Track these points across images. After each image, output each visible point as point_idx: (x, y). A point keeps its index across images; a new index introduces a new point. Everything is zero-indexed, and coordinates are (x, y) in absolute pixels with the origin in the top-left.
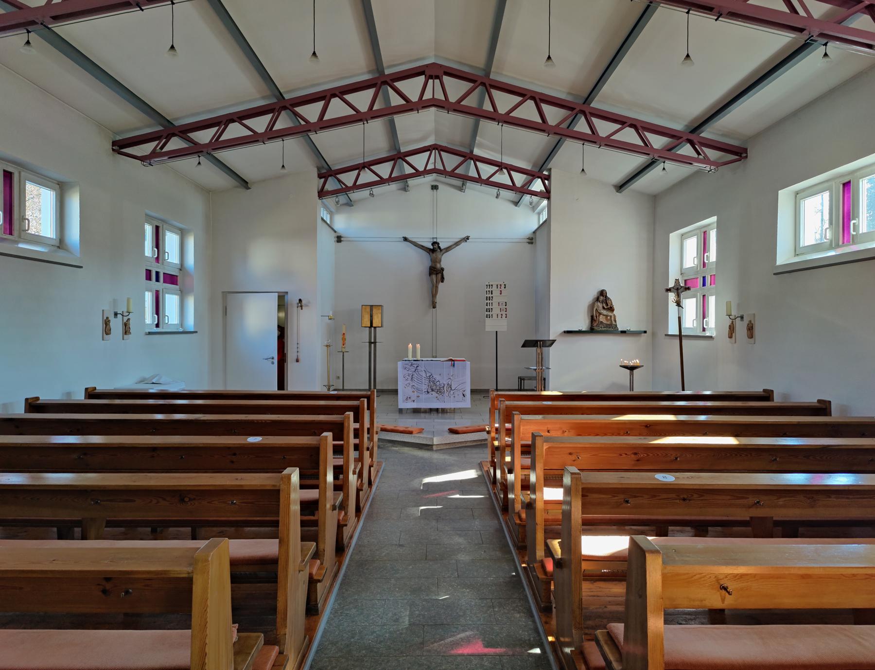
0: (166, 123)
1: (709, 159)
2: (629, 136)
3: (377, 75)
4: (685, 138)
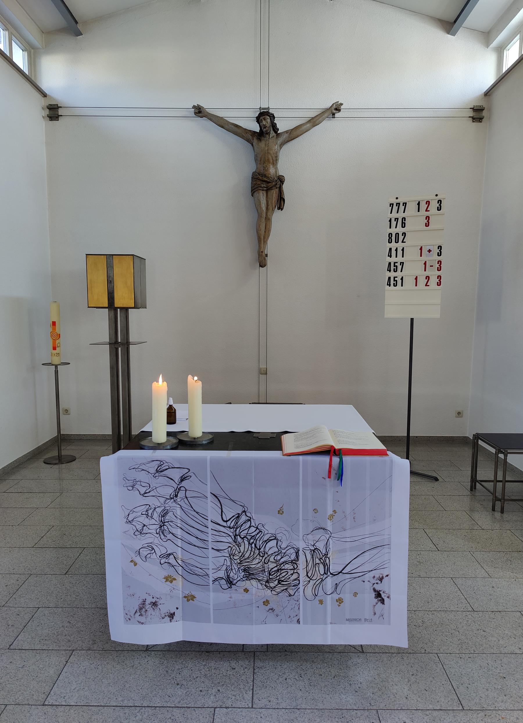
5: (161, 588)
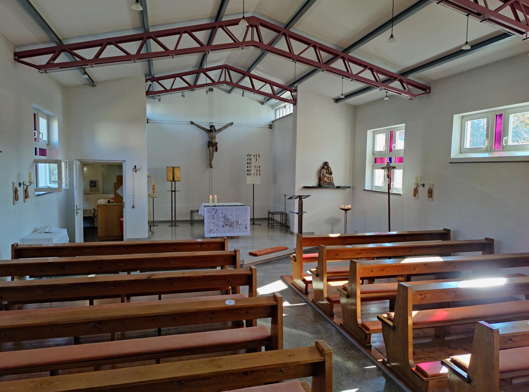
0: (58, 41)
5: (213, 228)
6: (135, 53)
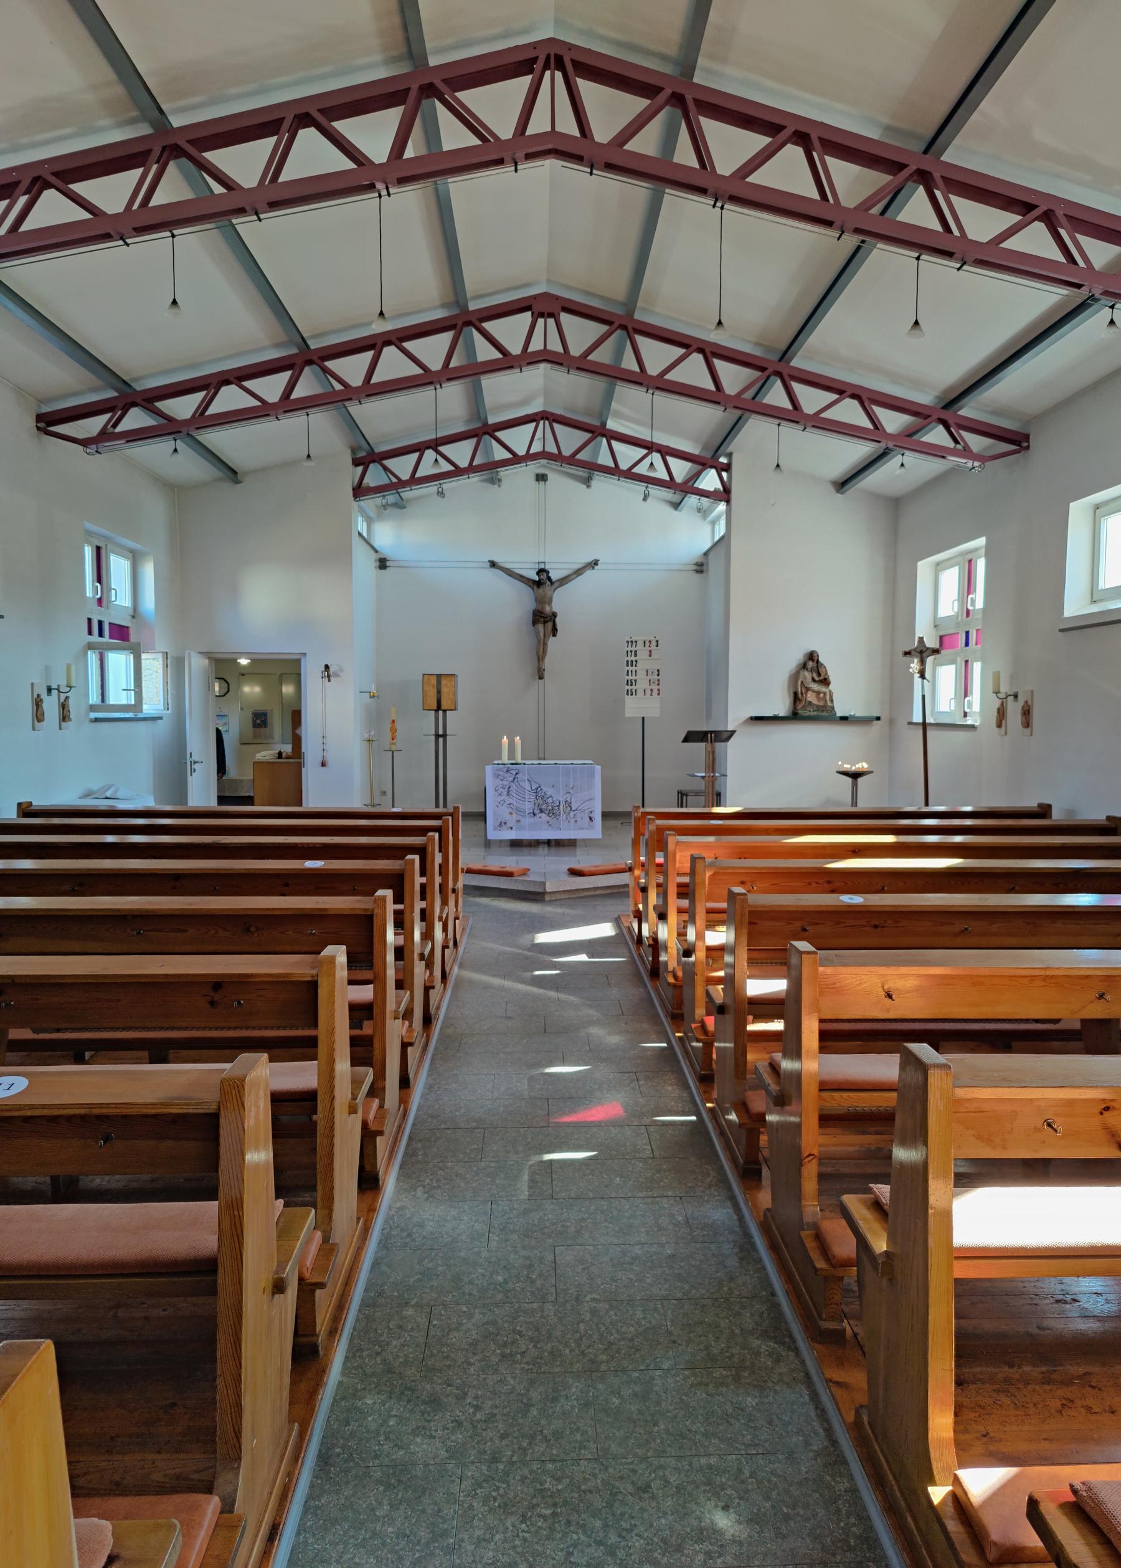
1: (971, 451)
2: (850, 412)
3: (455, 311)
4: (935, 417)
5: (507, 817)
6: (811, 413)
